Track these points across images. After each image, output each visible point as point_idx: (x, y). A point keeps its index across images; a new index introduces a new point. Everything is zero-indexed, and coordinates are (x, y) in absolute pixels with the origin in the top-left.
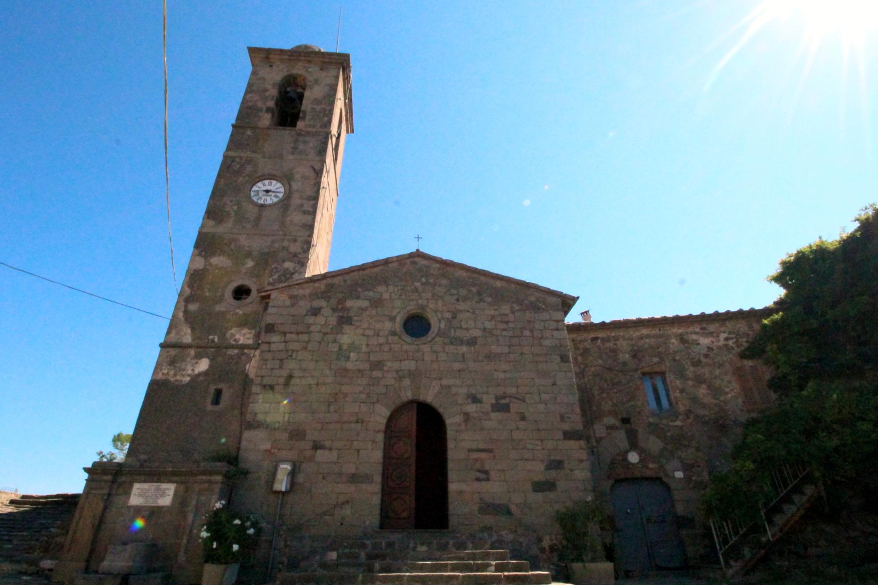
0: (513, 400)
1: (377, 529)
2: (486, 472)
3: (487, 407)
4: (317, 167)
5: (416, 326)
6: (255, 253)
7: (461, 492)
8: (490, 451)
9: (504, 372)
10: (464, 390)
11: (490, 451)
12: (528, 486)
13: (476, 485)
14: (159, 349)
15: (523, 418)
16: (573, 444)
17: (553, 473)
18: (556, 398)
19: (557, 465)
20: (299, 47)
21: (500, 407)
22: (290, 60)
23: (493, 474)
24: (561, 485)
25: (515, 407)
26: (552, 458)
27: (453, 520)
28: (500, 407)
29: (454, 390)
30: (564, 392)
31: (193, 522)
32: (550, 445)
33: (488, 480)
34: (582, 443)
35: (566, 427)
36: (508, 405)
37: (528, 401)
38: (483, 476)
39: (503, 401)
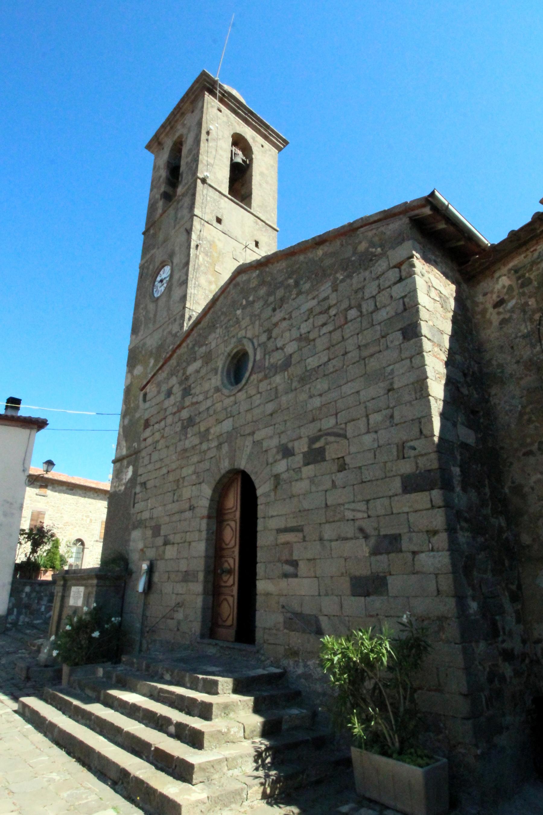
0: (331, 439)
1: (199, 639)
2: (295, 564)
3: (298, 459)
4: (188, 228)
5: (237, 368)
6: (154, 351)
7: (268, 594)
8: (297, 529)
9: (320, 395)
10: (275, 442)
11: (297, 529)
12: (345, 585)
13: (283, 583)
14: (112, 465)
15: (342, 467)
16: (421, 499)
17: (381, 563)
18: (392, 417)
19: (390, 544)
20: (534, 216)
21: (315, 456)
22: (171, 128)
23: (303, 567)
24: (394, 583)
25: (331, 453)
26: (382, 533)
27: (259, 635)
28: (315, 456)
29: (265, 445)
30: (407, 398)
31: (26, 634)
32: (379, 507)
33: (296, 576)
34: (436, 494)
35: (406, 467)
36: (322, 450)
37: (349, 435)
38: (289, 569)
39: (317, 445)
